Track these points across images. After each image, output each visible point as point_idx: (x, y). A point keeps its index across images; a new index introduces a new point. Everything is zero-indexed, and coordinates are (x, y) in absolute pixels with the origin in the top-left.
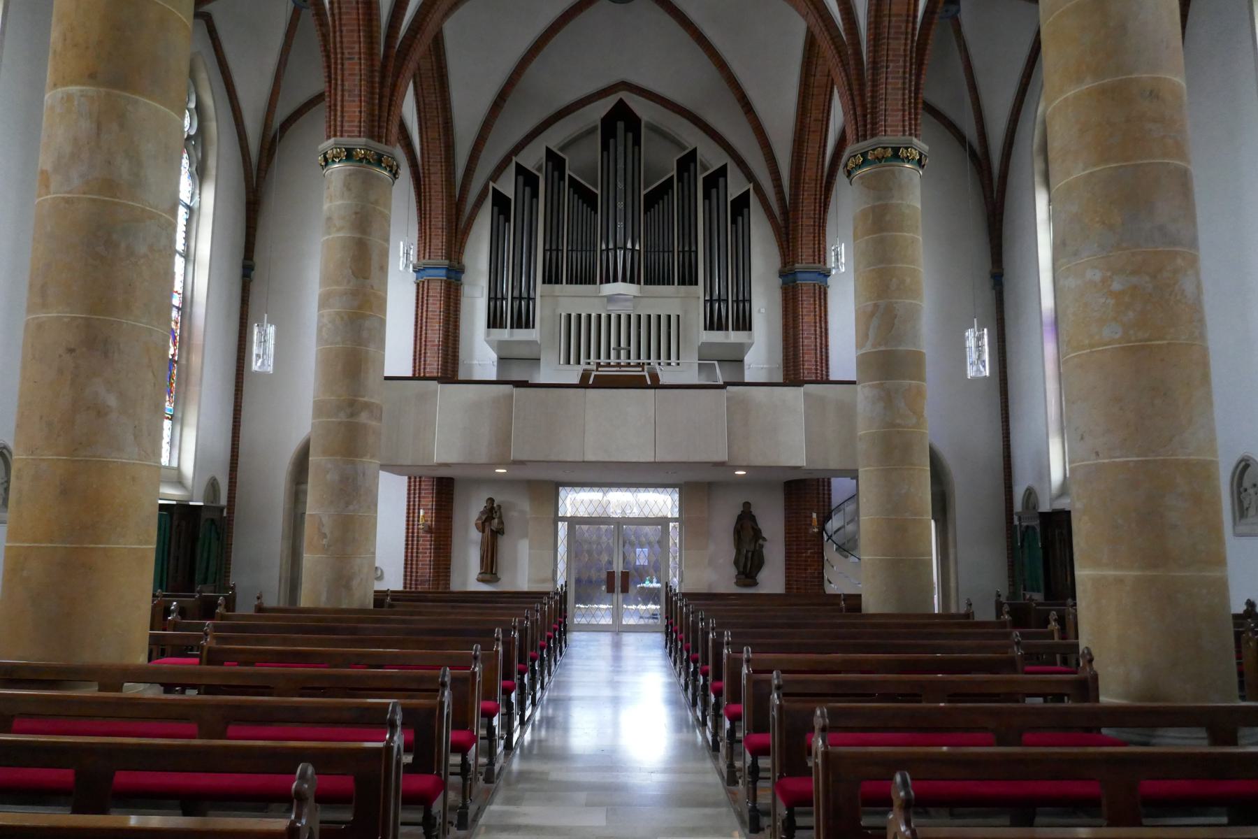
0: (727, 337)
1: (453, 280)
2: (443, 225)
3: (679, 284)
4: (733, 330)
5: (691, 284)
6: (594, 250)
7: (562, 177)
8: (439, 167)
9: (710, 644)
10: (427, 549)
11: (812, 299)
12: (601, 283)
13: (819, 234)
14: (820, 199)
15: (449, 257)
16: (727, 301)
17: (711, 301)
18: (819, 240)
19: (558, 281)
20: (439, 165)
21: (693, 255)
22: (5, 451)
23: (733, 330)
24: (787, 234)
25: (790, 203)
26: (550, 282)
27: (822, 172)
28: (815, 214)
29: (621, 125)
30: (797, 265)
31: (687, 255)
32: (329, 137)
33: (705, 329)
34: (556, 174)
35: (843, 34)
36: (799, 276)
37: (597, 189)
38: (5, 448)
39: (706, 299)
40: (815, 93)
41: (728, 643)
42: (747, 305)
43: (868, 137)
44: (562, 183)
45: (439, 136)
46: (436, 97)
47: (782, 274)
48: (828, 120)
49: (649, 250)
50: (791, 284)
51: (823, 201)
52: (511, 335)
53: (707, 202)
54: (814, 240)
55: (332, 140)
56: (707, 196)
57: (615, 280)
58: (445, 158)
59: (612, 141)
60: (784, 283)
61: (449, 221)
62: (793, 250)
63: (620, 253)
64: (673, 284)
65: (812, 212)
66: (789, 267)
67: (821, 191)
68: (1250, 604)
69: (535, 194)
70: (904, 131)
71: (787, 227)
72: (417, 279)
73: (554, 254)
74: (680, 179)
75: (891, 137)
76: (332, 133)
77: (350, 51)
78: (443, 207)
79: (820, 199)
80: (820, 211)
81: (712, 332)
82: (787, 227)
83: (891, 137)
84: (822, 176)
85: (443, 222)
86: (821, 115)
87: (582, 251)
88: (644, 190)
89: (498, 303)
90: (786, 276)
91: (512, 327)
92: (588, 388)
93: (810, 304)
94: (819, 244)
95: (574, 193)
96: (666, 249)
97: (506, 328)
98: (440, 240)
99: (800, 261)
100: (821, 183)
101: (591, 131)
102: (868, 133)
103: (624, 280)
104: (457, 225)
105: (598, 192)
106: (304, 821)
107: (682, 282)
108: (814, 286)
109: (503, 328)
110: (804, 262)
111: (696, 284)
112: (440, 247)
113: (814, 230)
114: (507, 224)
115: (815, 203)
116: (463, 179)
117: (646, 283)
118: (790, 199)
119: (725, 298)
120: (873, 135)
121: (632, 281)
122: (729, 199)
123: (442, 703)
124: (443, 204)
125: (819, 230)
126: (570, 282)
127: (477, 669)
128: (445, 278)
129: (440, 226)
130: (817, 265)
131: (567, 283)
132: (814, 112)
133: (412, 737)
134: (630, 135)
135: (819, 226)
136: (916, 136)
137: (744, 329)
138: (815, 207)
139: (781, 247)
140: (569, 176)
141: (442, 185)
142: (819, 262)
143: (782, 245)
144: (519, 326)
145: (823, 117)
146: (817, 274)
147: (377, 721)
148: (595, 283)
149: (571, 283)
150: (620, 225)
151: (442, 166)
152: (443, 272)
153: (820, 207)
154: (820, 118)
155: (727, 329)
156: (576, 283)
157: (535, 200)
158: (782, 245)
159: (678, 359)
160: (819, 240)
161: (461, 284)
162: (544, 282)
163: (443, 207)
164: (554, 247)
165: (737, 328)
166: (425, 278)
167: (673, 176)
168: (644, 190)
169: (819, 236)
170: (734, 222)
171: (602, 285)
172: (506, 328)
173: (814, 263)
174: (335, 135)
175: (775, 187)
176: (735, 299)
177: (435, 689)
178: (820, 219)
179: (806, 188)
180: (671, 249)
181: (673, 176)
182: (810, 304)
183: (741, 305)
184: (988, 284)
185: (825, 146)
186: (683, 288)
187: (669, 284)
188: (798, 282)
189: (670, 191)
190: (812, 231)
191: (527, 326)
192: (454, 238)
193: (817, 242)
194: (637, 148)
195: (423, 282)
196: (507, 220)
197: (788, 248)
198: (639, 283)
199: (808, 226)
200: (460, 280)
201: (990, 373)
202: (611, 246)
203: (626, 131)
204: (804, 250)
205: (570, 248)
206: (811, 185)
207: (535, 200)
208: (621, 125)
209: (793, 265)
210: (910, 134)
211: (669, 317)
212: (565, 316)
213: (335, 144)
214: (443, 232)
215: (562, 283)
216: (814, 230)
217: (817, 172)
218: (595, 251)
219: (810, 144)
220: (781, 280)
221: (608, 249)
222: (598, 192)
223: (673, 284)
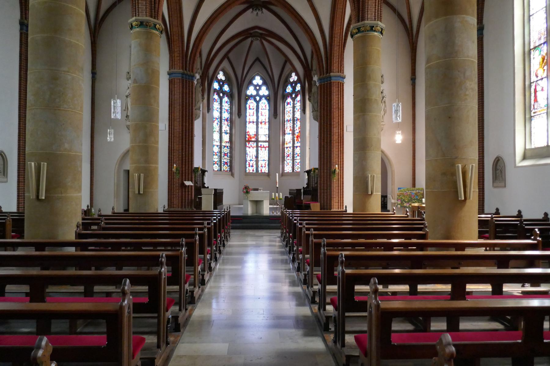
9: (345, 276)
10: (177, 193)
22: (2, 153)
32: (133, 16)
35: (305, 63)
38: (2, 152)
41: (342, 262)
43: (360, 21)
50: (326, 82)
55: (134, 18)
67: (342, 44)
68: (546, 214)
70: (375, 19)
72: (169, 78)
75: (369, 22)
76: (134, 15)
77: (274, 243)
83: (369, 22)
102: (360, 19)
106: (126, 302)
120: (362, 21)
123: (196, 240)
127: (206, 230)
130: (339, 74)
133: (187, 248)
136: (380, 21)
142: (341, 72)
147: (155, 261)
166: (173, 77)
174: (136, 16)
177: (193, 236)
184: (410, 82)
185: (344, 20)
195: (172, 80)
201: (402, 121)
209: (330, 73)
210: (378, 20)
213: (136, 20)
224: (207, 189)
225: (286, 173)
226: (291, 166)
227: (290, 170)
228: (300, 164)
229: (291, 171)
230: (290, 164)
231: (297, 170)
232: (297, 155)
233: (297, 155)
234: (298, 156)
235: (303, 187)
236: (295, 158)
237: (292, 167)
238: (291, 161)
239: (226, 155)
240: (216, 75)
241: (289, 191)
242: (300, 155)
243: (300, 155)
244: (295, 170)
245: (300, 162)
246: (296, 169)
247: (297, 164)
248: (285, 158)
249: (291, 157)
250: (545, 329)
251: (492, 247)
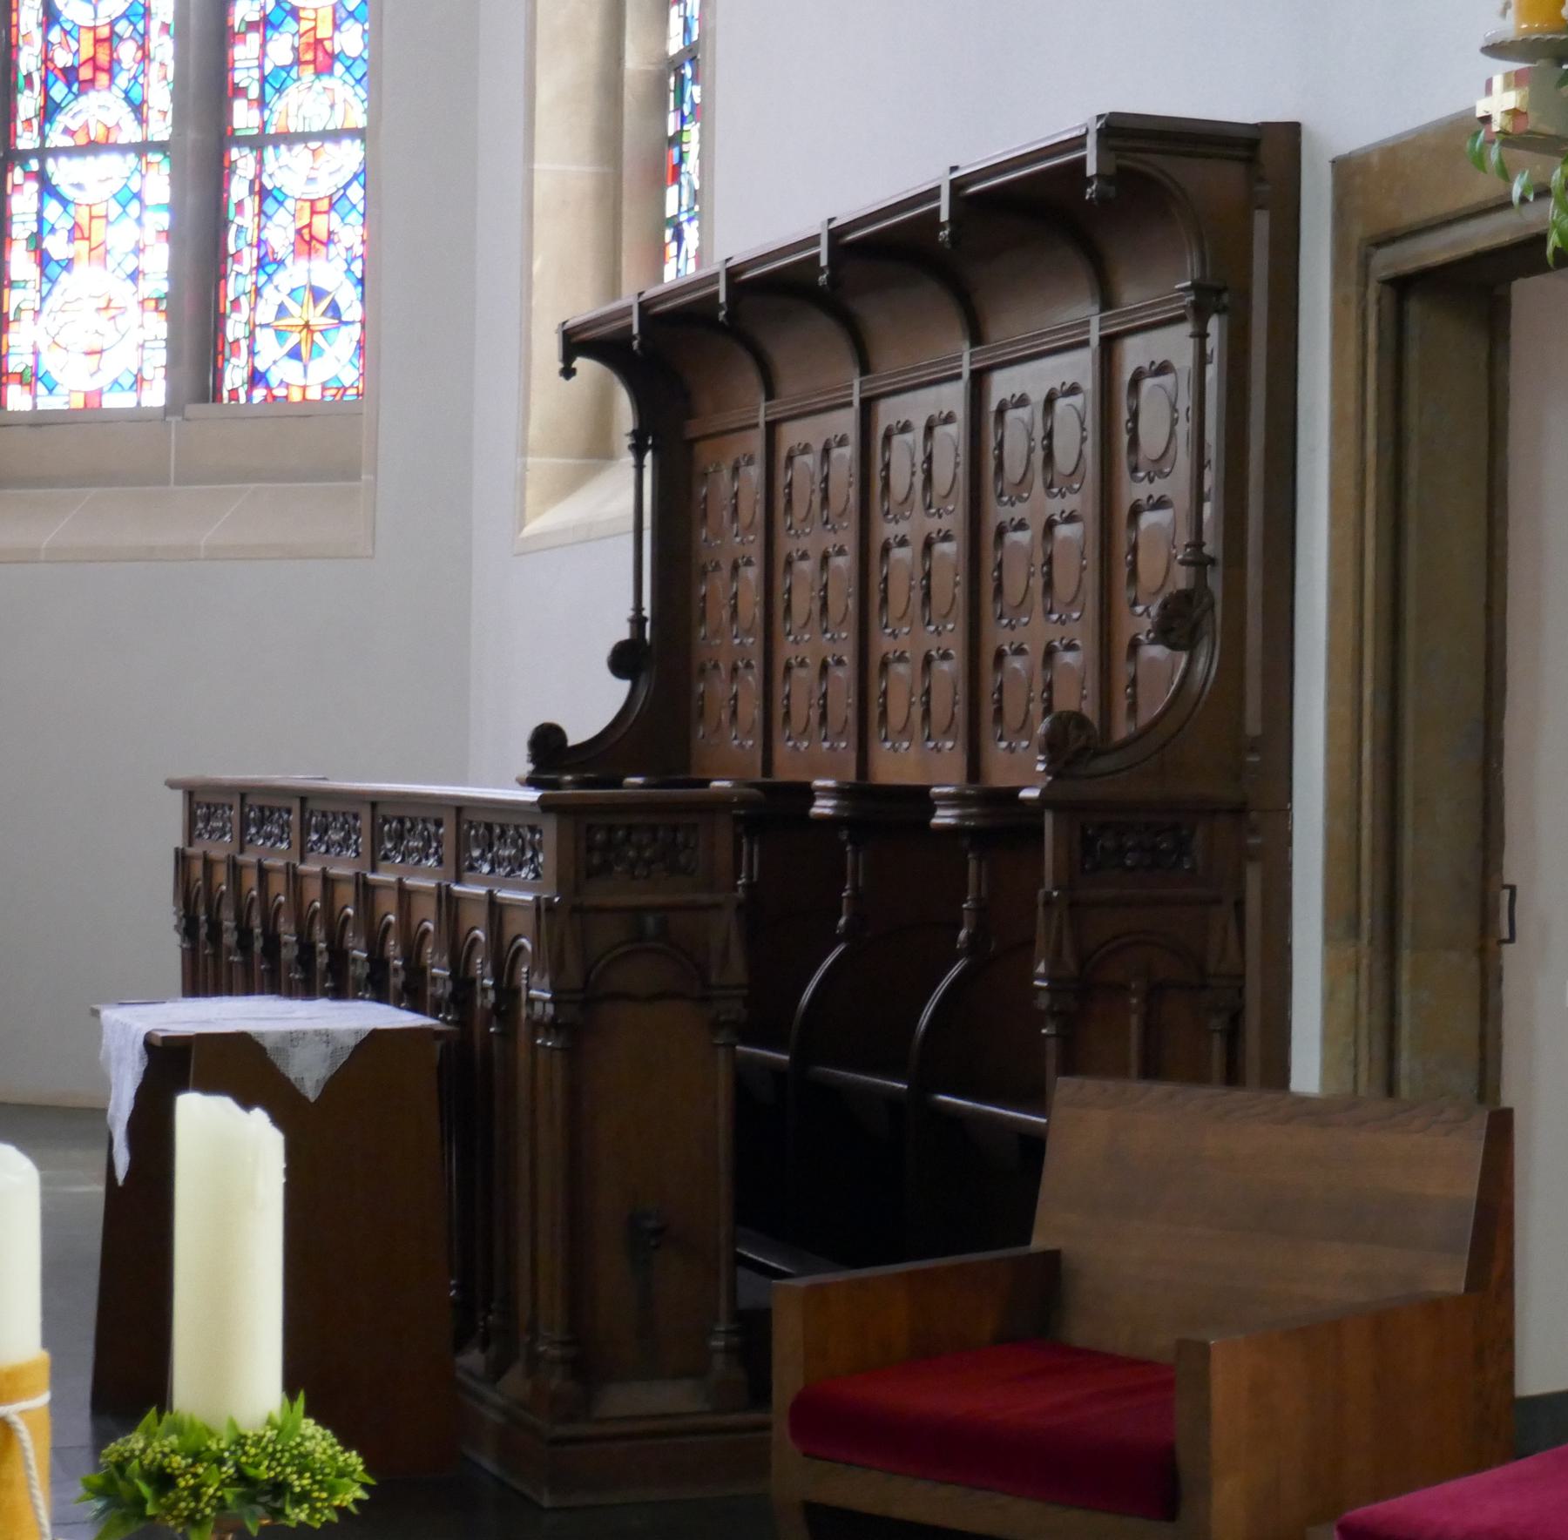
224: (23, 290)
225: (39, 421)
226: (157, 283)
227: (121, 362)
228: (351, 233)
229: (155, 396)
230: (120, 236)
231: (287, 376)
232: (281, 49)
233: (281, 49)
234: (319, 56)
235: (547, 742)
236: (244, 117)
237: (171, 306)
238: (158, 182)
239: (262, 186)
240: (230, 82)
241: (170, 830)
242: (351, 41)
243: (351, 41)
244: (234, 375)
245: (404, 967)
246: (269, 352)
247: (280, 236)
248: (28, 104)
249: (160, 97)
250: (1187, 584)
251: (952, 369)
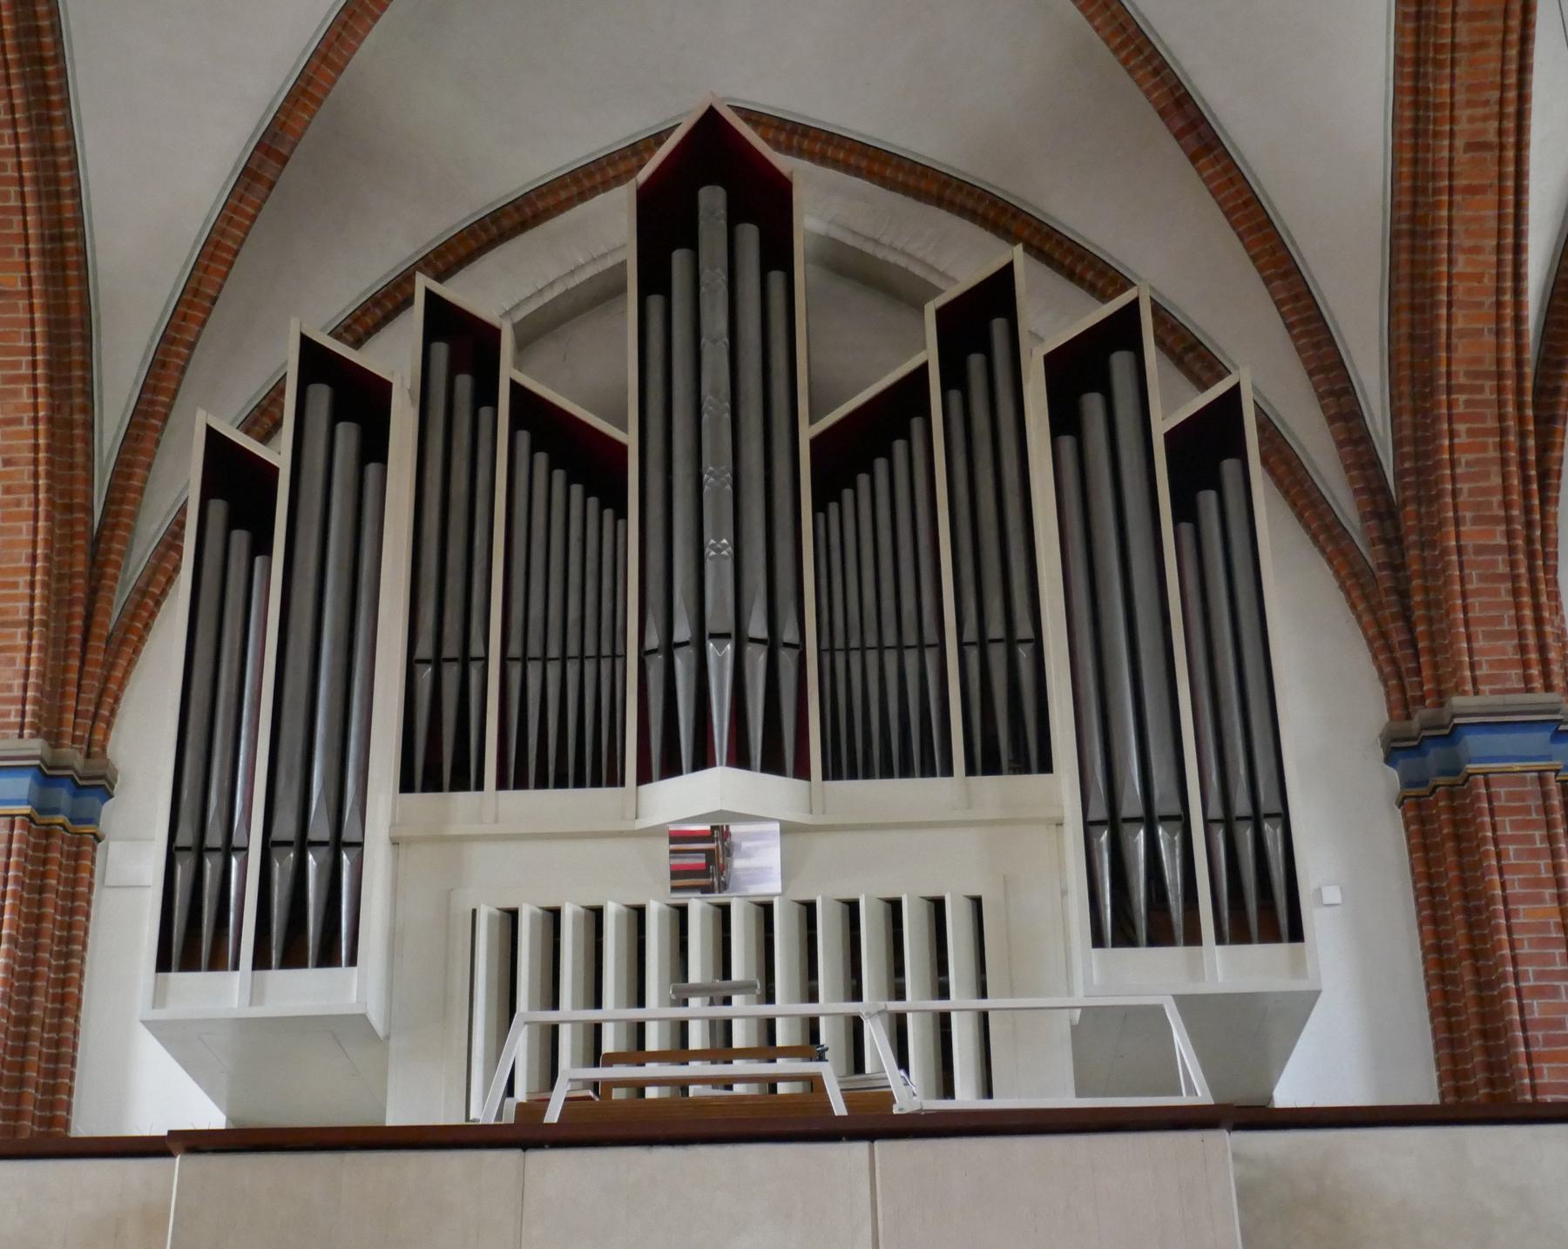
0: (1195, 971)
1: (60, 819)
2: (31, 611)
3: (970, 770)
4: (1220, 940)
5: (1021, 766)
6: (614, 656)
7: (485, 394)
8: (26, 399)
11: (1538, 834)
12: (644, 777)
13: (1533, 581)
14: (1523, 451)
15: (50, 728)
16: (1184, 820)
17: (1114, 822)
18: (1537, 607)
19: (464, 778)
20: (25, 388)
21: (1024, 653)
23: (1220, 940)
24: (1403, 594)
25: (1398, 475)
26: (433, 784)
27: (1519, 348)
28: (1507, 505)
29: (712, 201)
30: (1457, 701)
31: (997, 654)
33: (1098, 941)
34: (464, 382)
36: (1474, 743)
37: (624, 427)
39: (1092, 817)
40: (1463, 38)
42: (1271, 832)
44: (485, 412)
45: (29, 281)
46: (16, 138)
47: (1395, 749)
48: (1521, 146)
49: (839, 643)
51: (1532, 457)
52: (256, 996)
53: (1067, 442)
54: (1518, 607)
56: (1065, 420)
57: (703, 760)
58: (49, 365)
59: (679, 258)
60: (1407, 783)
61: (58, 599)
62: (1433, 652)
63: (720, 656)
64: (948, 771)
65: (1497, 499)
66: (1421, 714)
69: (374, 448)
71: (1396, 567)
73: (451, 673)
74: (954, 376)
78: (34, 544)
79: (1523, 451)
80: (1526, 495)
81: (1250, 263)
82: (1396, 567)
84: (1519, 363)
85: (32, 599)
86: (1493, 125)
87: (564, 658)
88: (812, 422)
89: (211, 865)
90: (1418, 750)
91: (261, 961)
92: (538, 1144)
93: (1535, 854)
94: (1539, 621)
95: (534, 449)
96: (910, 638)
97: (236, 967)
98: (20, 665)
99: (1469, 687)
100: (1520, 391)
101: (604, 292)
103: (739, 759)
104: (89, 618)
105: (631, 439)
107: (986, 762)
108: (1542, 780)
109: (225, 968)
110: (1484, 688)
111: (1046, 766)
112: (17, 693)
113: (1513, 564)
114: (258, 560)
115: (1504, 462)
116: (123, 450)
117: (833, 771)
118: (1399, 458)
119: (1175, 809)
121: (772, 764)
122: (1161, 426)
124: (35, 531)
125: (1531, 569)
126: (514, 777)
128: (26, 809)
129: (22, 616)
131: (502, 784)
132: (1463, 114)
134: (749, 235)
135: (1531, 555)
137: (1270, 934)
138: (1505, 476)
139: (1380, 643)
140: (515, 386)
141: (36, 462)
143: (1384, 635)
144: (293, 958)
145: (1501, 132)
146: (1545, 735)
148: (616, 780)
149: (521, 784)
150: (719, 547)
151: (35, 393)
152: (21, 786)
153: (1525, 480)
154: (1492, 137)
155: (1193, 937)
156: (542, 784)
157: (372, 469)
158: (1384, 635)
159: (983, 993)
160: (1537, 607)
161: (98, 839)
162: (406, 785)
163: (34, 544)
164: (451, 649)
165: (1236, 931)
167: (924, 368)
168: (812, 422)
169: (1535, 594)
170: (1185, 511)
171: (645, 788)
172: (236, 967)
173: (1529, 690)
175: (1331, 420)
176: (1216, 811)
178: (1529, 525)
179: (1460, 409)
180: (930, 636)
181: (924, 368)
182: (1535, 854)
183: (1246, 835)
186: (988, 785)
187: (928, 771)
188: (1471, 767)
189: (917, 424)
190: (1503, 569)
191: (328, 957)
192: (75, 663)
193: (1528, 612)
194: (776, 278)
196: (261, 546)
197: (1413, 643)
198: (802, 772)
199: (1480, 550)
200: (93, 820)
202: (682, 632)
203: (733, 220)
204: (1480, 644)
205: (515, 649)
206: (1471, 457)
207: (372, 469)
208: (712, 201)
209: (1441, 696)
211: (938, 905)
212: (490, 917)
214: (30, 637)
215: (480, 786)
216: (1513, 564)
217: (1499, 348)
218: (618, 656)
219: (1461, 240)
220: (1394, 774)
221: (669, 647)
222: (631, 439)
223: (948, 771)
